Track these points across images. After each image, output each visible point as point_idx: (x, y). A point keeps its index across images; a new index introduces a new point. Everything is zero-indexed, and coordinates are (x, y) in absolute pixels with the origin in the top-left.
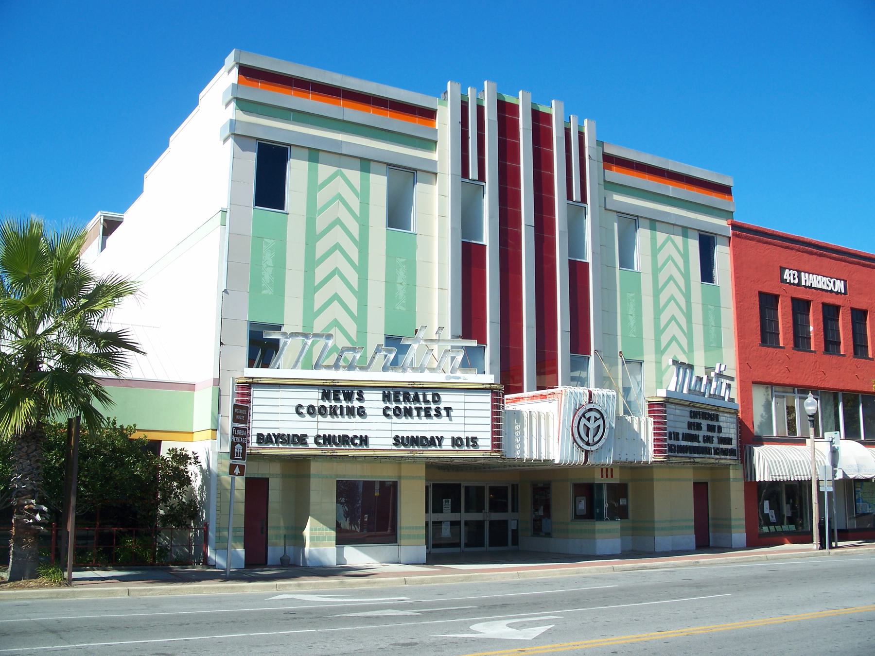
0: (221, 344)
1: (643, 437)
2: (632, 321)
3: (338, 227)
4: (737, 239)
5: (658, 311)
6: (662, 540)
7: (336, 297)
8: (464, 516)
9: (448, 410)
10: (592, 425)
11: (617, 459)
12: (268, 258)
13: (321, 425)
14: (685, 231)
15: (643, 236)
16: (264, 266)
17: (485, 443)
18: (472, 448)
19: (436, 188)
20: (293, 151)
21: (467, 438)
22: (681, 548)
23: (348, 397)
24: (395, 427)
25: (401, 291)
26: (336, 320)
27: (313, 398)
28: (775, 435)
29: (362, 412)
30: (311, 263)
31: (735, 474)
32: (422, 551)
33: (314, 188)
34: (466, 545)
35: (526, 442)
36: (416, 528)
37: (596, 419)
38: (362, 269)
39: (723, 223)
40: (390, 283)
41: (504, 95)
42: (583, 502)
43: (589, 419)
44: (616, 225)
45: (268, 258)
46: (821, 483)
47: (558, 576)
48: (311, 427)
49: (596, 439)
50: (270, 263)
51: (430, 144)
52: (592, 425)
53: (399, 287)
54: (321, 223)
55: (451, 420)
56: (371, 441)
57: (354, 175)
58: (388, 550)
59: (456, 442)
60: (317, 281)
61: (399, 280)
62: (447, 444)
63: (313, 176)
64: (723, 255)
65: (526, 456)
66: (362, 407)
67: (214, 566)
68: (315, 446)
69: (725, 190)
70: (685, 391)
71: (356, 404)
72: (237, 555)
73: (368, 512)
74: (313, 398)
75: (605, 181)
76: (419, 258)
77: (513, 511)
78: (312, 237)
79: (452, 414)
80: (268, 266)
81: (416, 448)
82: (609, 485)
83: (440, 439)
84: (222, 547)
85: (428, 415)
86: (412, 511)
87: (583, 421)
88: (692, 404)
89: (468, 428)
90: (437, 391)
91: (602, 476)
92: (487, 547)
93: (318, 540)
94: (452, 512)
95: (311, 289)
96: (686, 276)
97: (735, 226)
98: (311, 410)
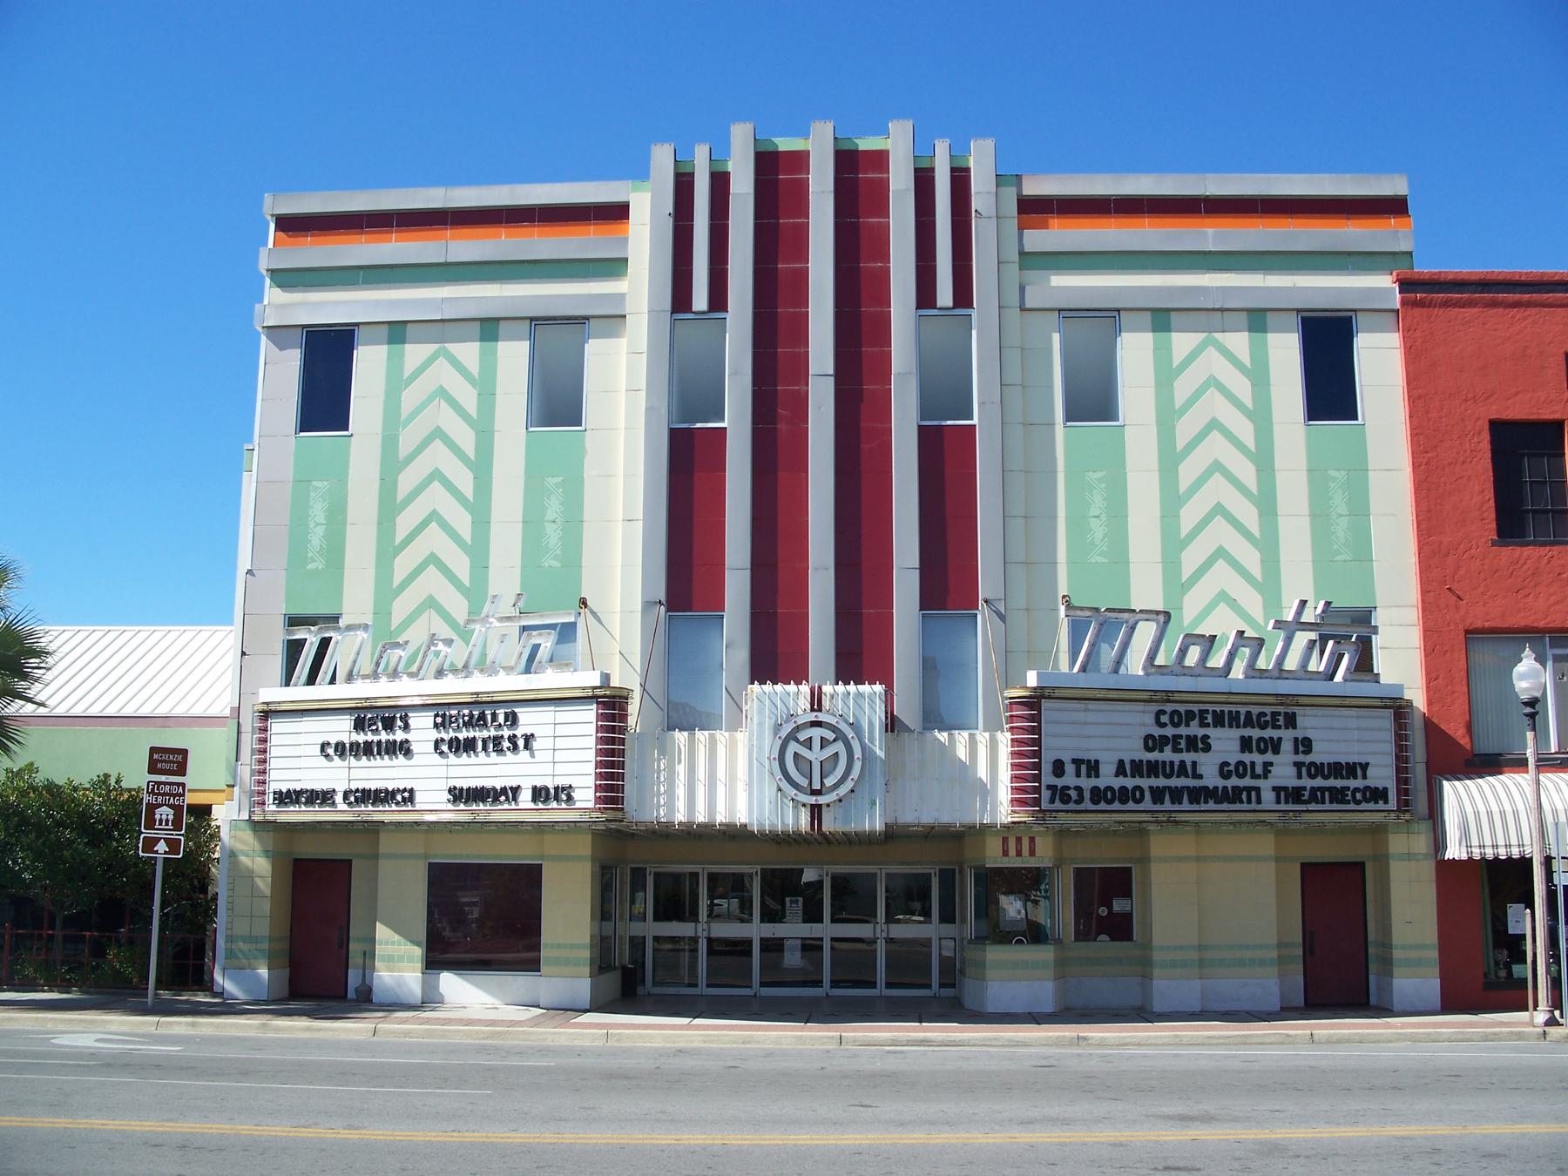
0: (243, 654)
1: (982, 772)
2: (1098, 529)
3: (1215, 434)
4: (1417, 311)
5: (1172, 501)
6: (1165, 988)
8: (826, 930)
9: (528, 739)
10: (816, 755)
11: (889, 821)
12: (318, 512)
14: (1257, 319)
16: (312, 525)
17: (586, 797)
18: (564, 805)
19: (622, 344)
20: (1361, 321)
21: (556, 789)
23: (389, 725)
24: (453, 772)
25: (553, 534)
26: (431, 597)
27: (341, 729)
28: (1554, 748)
29: (404, 749)
30: (389, 506)
31: (1406, 844)
32: (582, 987)
33: (1166, 374)
34: (835, 984)
35: (681, 791)
36: (573, 946)
37: (824, 743)
38: (480, 509)
39: (1383, 283)
40: (532, 523)
41: (776, 140)
43: (808, 744)
44: (1056, 337)
45: (318, 512)
46: (1555, 865)
48: (339, 776)
49: (829, 782)
50: (321, 518)
51: (615, 266)
52: (816, 755)
53: (550, 528)
54: (407, 440)
55: (532, 756)
56: (418, 797)
57: (1239, 341)
58: (519, 982)
59: (539, 794)
61: (550, 515)
62: (525, 797)
63: (1162, 356)
64: (1379, 360)
65: (680, 817)
66: (1207, 737)
67: (220, 995)
68: (345, 807)
69: (1394, 207)
70: (1238, 672)
71: (399, 736)
72: (258, 978)
73: (482, 915)
74: (341, 729)
75: (1022, 253)
76: (590, 470)
78: (392, 464)
79: (536, 745)
81: (481, 807)
83: (516, 790)
84: (236, 966)
85: (500, 751)
86: (567, 915)
87: (793, 747)
88: (1167, 696)
89: (560, 769)
90: (511, 706)
91: (1005, 853)
93: (396, 960)
95: (387, 551)
96: (1261, 416)
97: (1406, 285)
98: (340, 749)
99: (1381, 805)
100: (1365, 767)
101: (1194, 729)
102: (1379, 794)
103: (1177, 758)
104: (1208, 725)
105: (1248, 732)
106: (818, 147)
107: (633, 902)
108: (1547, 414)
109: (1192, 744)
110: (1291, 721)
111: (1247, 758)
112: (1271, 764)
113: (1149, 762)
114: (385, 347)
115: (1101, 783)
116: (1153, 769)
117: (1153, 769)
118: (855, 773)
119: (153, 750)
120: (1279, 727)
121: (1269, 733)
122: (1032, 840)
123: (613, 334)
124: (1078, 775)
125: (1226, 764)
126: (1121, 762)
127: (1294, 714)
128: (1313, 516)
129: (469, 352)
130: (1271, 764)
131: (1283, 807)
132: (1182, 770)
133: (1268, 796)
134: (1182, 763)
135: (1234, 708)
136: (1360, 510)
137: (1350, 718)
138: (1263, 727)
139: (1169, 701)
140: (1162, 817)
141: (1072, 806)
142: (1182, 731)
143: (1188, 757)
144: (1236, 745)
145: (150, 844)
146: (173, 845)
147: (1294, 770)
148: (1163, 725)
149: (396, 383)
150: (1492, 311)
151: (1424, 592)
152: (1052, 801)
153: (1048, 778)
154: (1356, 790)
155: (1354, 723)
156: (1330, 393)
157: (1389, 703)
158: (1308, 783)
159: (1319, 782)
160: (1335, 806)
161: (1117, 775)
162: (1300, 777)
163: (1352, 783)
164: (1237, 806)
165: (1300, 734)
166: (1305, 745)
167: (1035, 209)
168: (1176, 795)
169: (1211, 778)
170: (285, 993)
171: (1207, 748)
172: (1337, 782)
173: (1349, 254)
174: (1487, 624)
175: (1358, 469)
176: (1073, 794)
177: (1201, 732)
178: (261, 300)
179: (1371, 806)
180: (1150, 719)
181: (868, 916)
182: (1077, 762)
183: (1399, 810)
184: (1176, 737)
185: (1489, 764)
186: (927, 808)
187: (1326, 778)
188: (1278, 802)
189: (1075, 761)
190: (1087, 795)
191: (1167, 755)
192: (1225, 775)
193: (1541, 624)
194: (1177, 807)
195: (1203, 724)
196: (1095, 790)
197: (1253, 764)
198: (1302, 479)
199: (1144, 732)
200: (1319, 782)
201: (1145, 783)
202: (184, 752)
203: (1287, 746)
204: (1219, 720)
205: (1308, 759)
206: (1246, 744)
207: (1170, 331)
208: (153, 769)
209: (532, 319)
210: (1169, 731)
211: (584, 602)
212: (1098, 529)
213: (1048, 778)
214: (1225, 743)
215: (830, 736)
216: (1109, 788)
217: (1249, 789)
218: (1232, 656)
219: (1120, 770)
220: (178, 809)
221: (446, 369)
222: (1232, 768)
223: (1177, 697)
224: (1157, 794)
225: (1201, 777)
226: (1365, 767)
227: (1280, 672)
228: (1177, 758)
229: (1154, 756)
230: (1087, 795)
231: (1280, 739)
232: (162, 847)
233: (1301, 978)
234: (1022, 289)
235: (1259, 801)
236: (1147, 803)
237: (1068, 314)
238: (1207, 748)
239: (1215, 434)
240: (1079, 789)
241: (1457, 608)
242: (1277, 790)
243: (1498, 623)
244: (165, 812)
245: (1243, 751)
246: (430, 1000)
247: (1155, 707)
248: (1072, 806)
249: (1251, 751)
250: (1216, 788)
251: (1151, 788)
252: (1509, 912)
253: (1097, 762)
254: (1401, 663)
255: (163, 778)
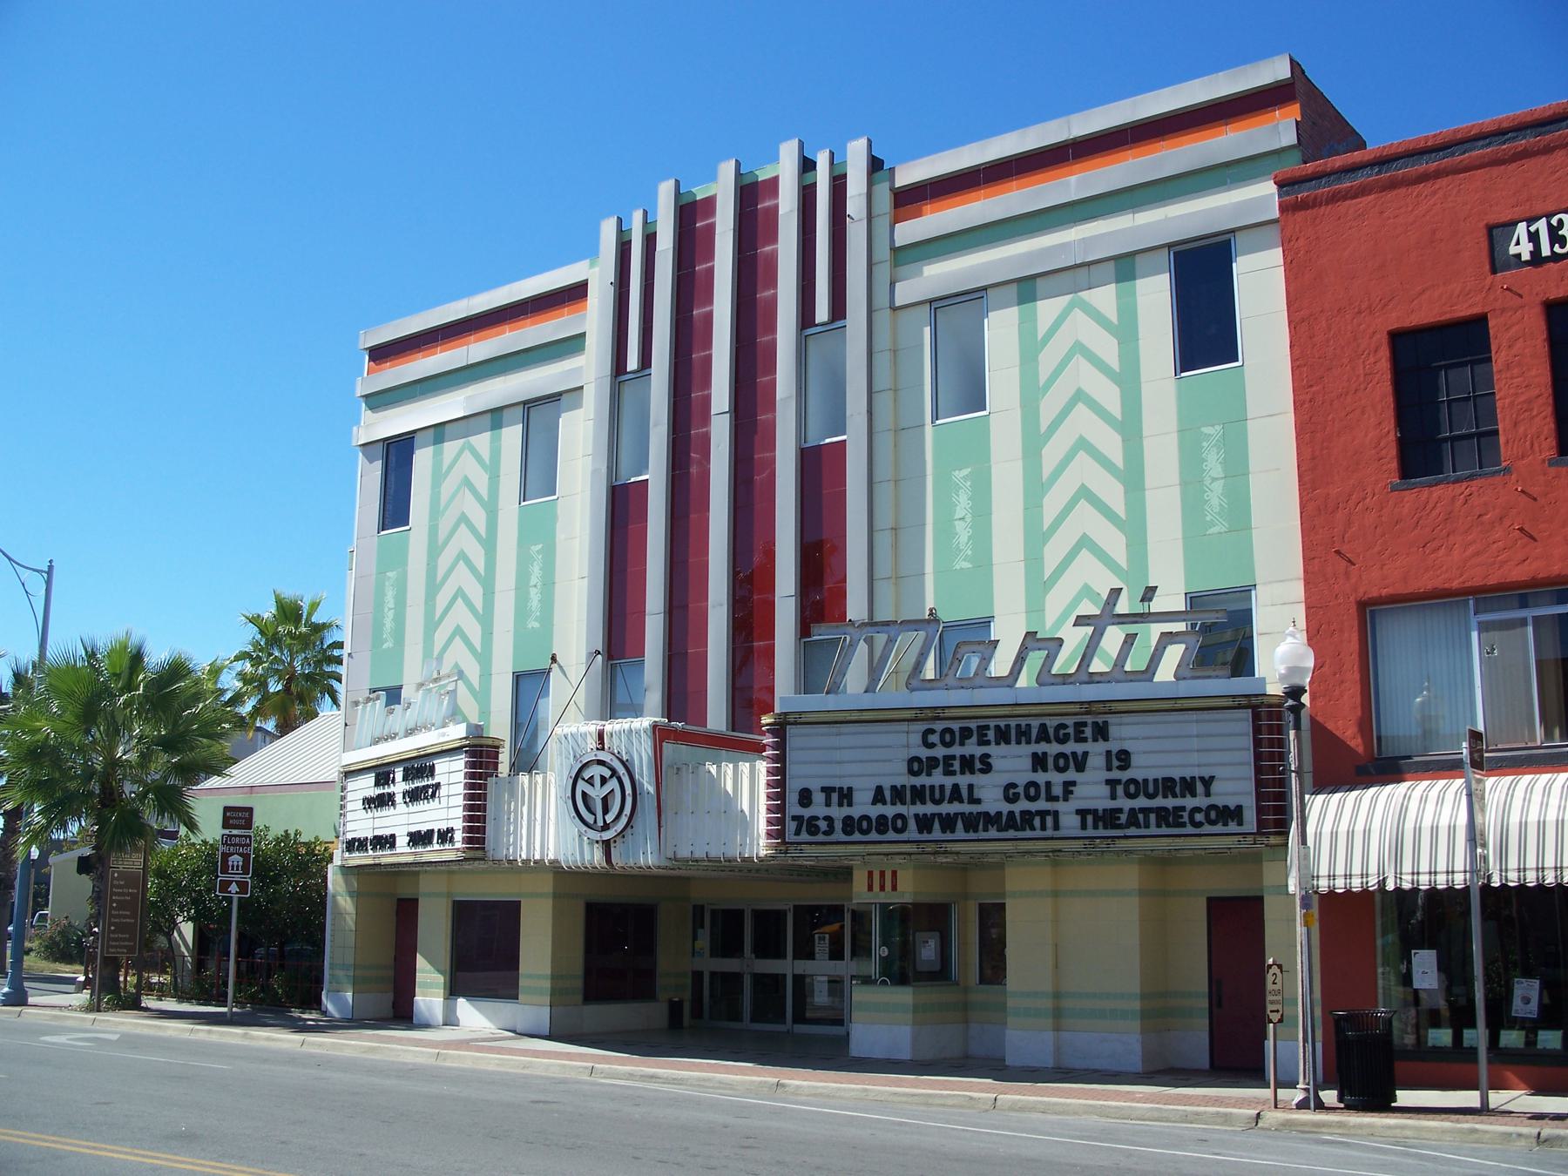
2: (963, 532)
3: (1080, 406)
4: (1300, 216)
5: (1035, 488)
7: (1085, 542)
10: (597, 793)
13: (378, 823)
15: (1000, 330)
16: (1207, 481)
19: (578, 414)
22: (1097, 1064)
25: (535, 596)
30: (433, 588)
37: (604, 781)
42: (932, 943)
43: (590, 781)
47: (491, 1068)
49: (609, 818)
50: (1217, 471)
52: (597, 793)
58: (505, 1008)
59: (418, 839)
60: (1048, 521)
62: (402, 841)
64: (1260, 286)
66: (987, 756)
76: (560, 536)
77: (854, 954)
78: (434, 551)
80: (1214, 479)
82: (884, 906)
87: (581, 786)
88: (936, 713)
91: (870, 888)
92: (746, 1023)
94: (831, 958)
96: (1128, 378)
99: (1232, 827)
100: (1208, 782)
101: (972, 748)
102: (1232, 814)
103: (949, 782)
104: (988, 743)
105: (1042, 748)
106: (723, 190)
107: (695, 938)
108: (1463, 311)
109: (967, 764)
110: (1101, 732)
111: (1041, 778)
112: (1073, 783)
113: (913, 787)
114: (1015, 309)
115: (856, 812)
116: (919, 794)
117: (919, 794)
118: (627, 810)
119: (226, 809)
120: (1085, 740)
121: (1070, 747)
122: (894, 873)
123: (577, 405)
124: (828, 804)
125: (1014, 785)
126: (879, 790)
127: (1106, 723)
128: (1184, 484)
129: (1104, 297)
130: (1073, 783)
131: (1090, 832)
132: (956, 794)
133: (1070, 822)
134: (956, 787)
135: (1023, 722)
136: (1237, 468)
137: (1192, 725)
138: (1062, 740)
139: (938, 718)
140: (930, 848)
141: (820, 838)
142: (957, 750)
143: (963, 780)
144: (1028, 763)
145: (225, 885)
146: (242, 886)
147: (1106, 790)
148: (931, 746)
149: (438, 477)
150: (1390, 195)
151: (1307, 560)
152: (798, 833)
153: (794, 808)
154: (1197, 810)
155: (1194, 729)
156: (1206, 333)
157: (1244, 702)
158: (1126, 804)
159: (1142, 802)
160: (1164, 830)
161: (874, 803)
162: (1113, 797)
163: (1189, 802)
164: (1028, 833)
165: (1114, 746)
166: (1124, 758)
167: (911, 199)
168: (948, 823)
169: (991, 799)
170: (391, 1015)
171: (987, 768)
172: (1170, 804)
173: (472, 365)
174: (1384, 592)
175: (1236, 422)
176: (823, 825)
177: (978, 751)
178: (358, 423)
179: (1219, 828)
180: (916, 739)
181: (780, 955)
182: (828, 790)
183: (1259, 833)
184: (948, 759)
185: (1380, 766)
186: (697, 841)
187: (1150, 796)
188: (1084, 826)
189: (824, 789)
190: (838, 825)
191: (937, 778)
192: (1010, 798)
193: (1455, 584)
194: (948, 836)
195: (983, 742)
196: (848, 820)
197: (1048, 784)
198: (1172, 441)
199: (906, 754)
200: (1142, 802)
201: (910, 810)
202: (250, 810)
203: (1096, 761)
204: (1003, 736)
205: (1125, 776)
206: (1039, 762)
207: (1035, 300)
208: (226, 825)
209: (931, 301)
210: (940, 752)
211: (554, 659)
212: (963, 532)
213: (794, 808)
214: (1012, 762)
215: (607, 773)
216: (866, 817)
217: (1043, 814)
218: (1020, 660)
219: (879, 797)
220: (246, 857)
221: (1079, 323)
222: (1021, 790)
223: (948, 713)
224: (924, 823)
225: (978, 801)
226: (1208, 782)
227: (1084, 675)
228: (949, 782)
229: (918, 781)
230: (838, 825)
231: (1086, 754)
232: (234, 888)
233: (1205, 1036)
234: (892, 285)
235: (1056, 827)
236: (912, 832)
237: (937, 304)
238: (987, 768)
239: (1080, 406)
240: (828, 819)
241: (1347, 575)
242: (1082, 813)
243: (1401, 589)
244: (236, 860)
245: (1035, 770)
246: (450, 1021)
247: (923, 727)
248: (820, 838)
249: (1045, 770)
250: (999, 814)
251: (916, 816)
252: (1414, 960)
253: (850, 789)
254: (1282, 653)
255: (235, 832)
